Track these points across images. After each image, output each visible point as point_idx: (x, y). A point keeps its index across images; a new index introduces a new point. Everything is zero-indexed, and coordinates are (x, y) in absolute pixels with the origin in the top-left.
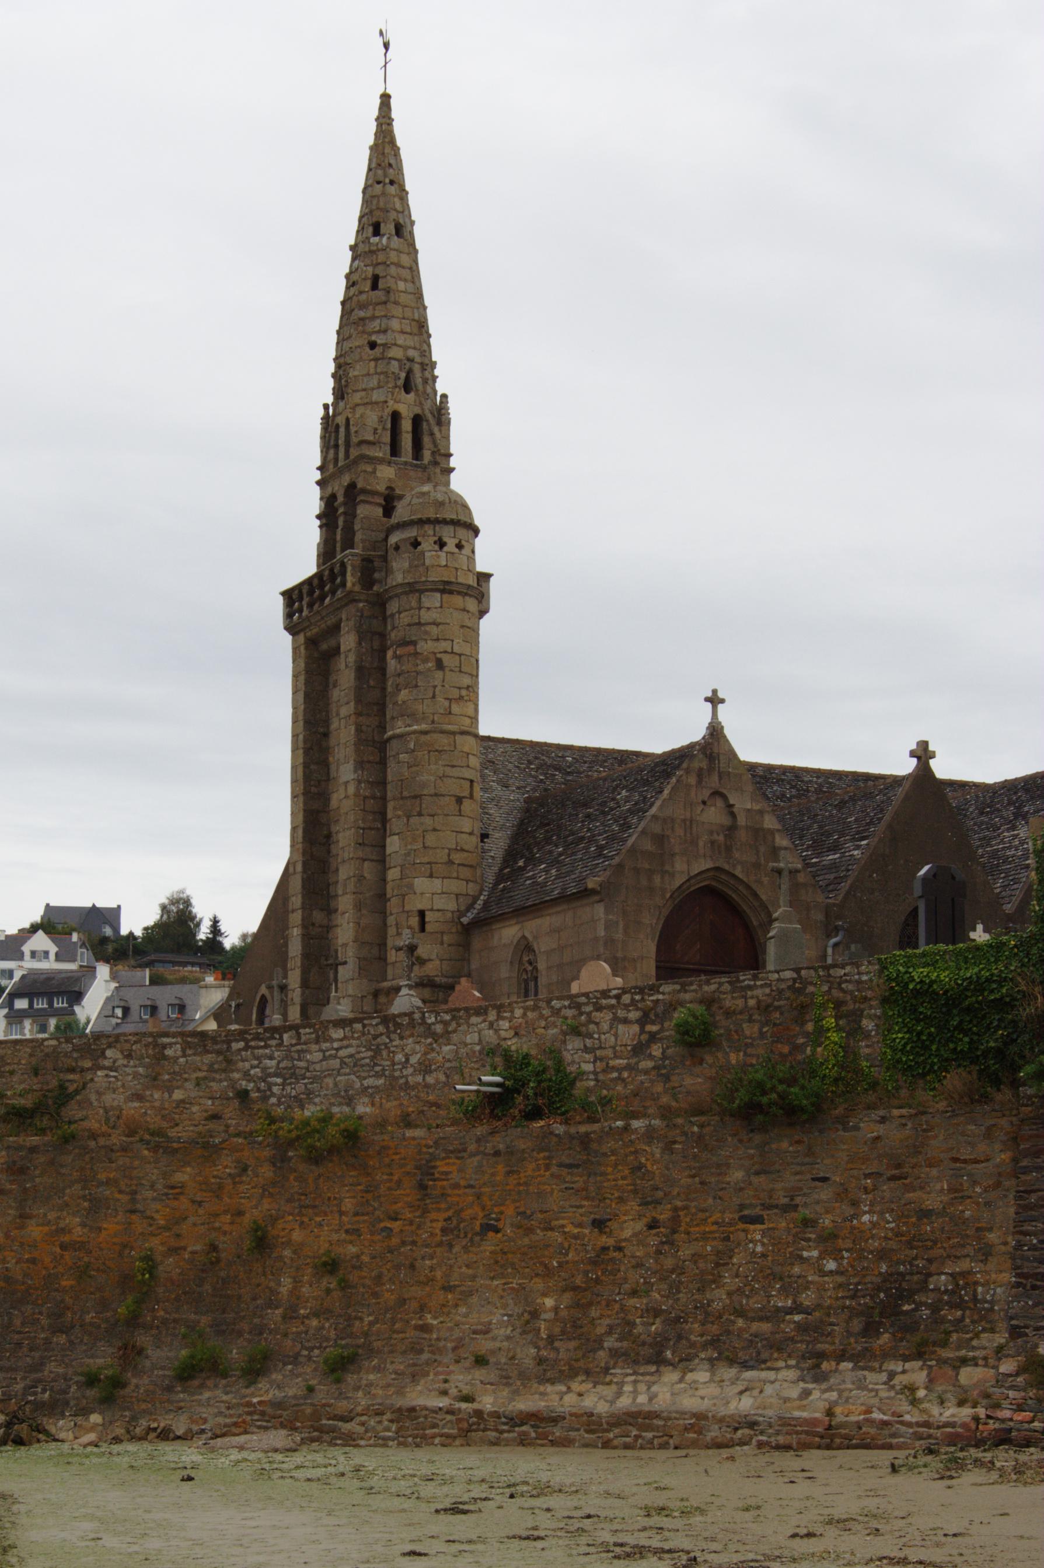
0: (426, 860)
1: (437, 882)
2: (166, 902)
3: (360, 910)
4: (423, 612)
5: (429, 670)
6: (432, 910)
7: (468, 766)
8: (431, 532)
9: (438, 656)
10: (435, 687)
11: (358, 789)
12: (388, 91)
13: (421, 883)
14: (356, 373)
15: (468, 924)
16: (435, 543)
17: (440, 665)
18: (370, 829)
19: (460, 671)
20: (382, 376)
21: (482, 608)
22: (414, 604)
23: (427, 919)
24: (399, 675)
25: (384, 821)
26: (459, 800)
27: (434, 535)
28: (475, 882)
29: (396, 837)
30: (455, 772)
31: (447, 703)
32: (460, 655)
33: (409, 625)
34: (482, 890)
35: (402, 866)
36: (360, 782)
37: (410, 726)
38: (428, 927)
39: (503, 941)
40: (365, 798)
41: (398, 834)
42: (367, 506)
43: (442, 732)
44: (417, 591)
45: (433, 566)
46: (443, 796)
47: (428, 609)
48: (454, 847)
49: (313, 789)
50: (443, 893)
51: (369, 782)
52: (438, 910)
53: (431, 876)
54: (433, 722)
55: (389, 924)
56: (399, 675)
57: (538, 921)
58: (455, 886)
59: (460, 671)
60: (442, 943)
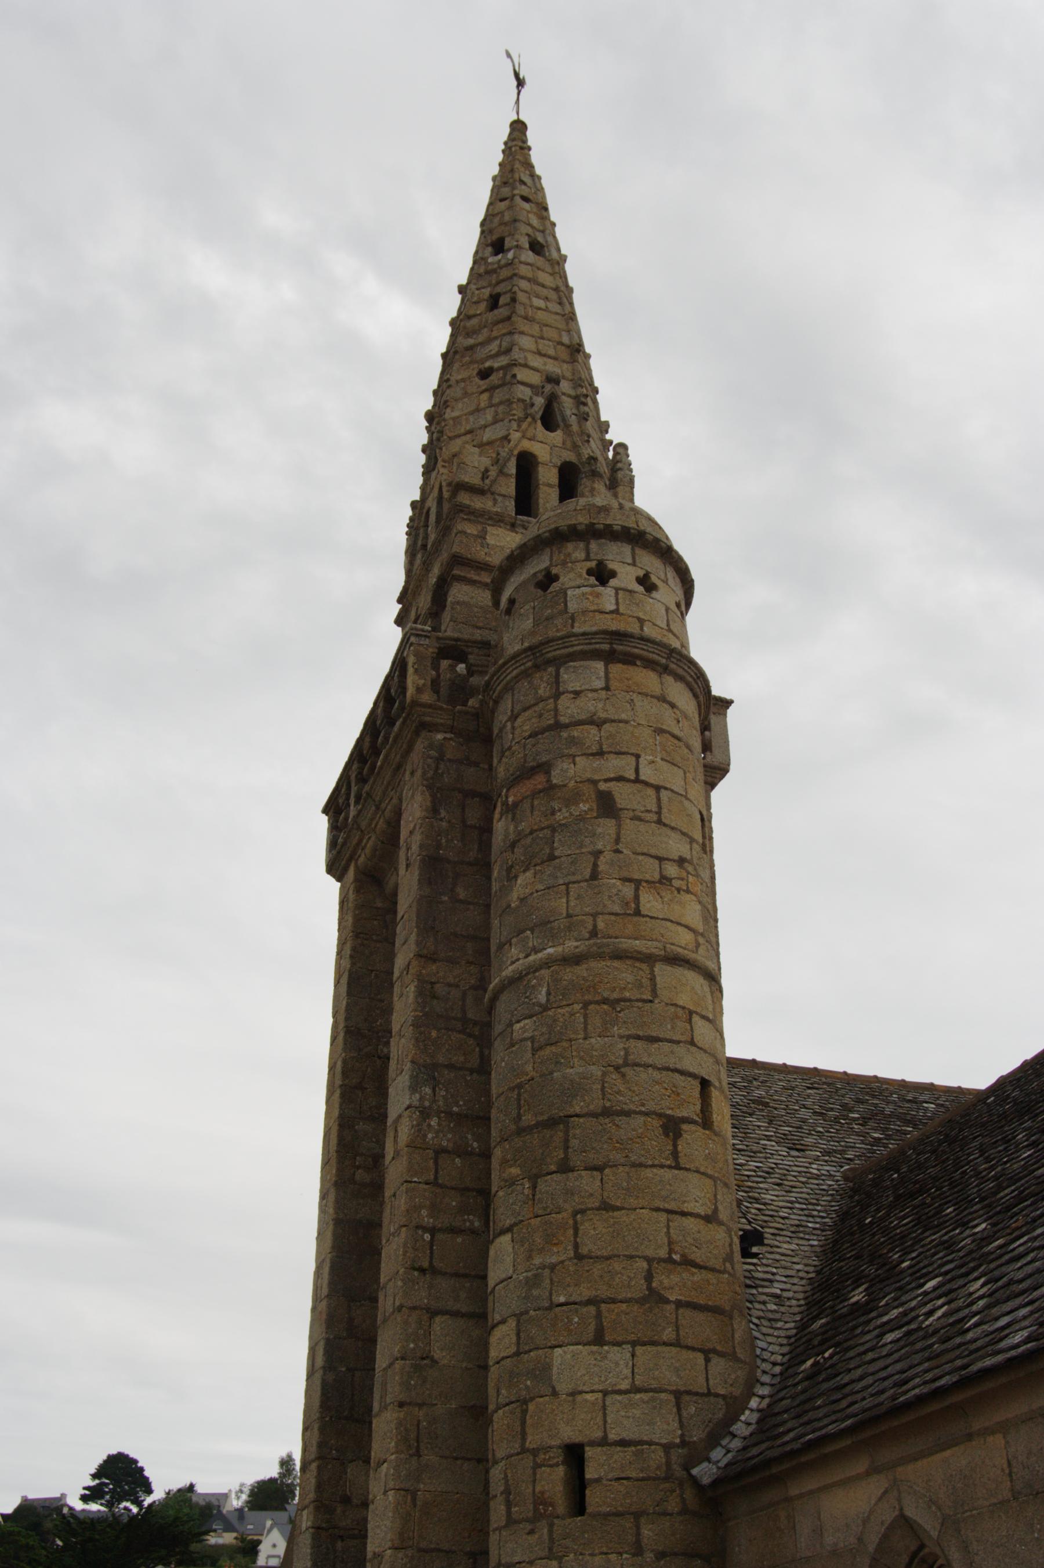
0: (585, 1292)
1: (619, 1356)
2: (139, 1465)
3: (418, 1454)
4: (564, 701)
5: (581, 818)
6: (603, 1442)
7: (692, 1043)
8: (580, 555)
9: (603, 786)
10: (597, 854)
11: (419, 1132)
12: (522, 118)
13: (571, 1363)
14: (456, 414)
15: (716, 1483)
16: (590, 572)
17: (607, 806)
18: (453, 1231)
19: (659, 822)
20: (501, 408)
21: (714, 759)
22: (544, 690)
23: (590, 1474)
24: (513, 845)
25: (482, 1197)
26: (672, 1127)
27: (588, 558)
28: (731, 1356)
29: (506, 1238)
30: (659, 1054)
31: (628, 890)
32: (658, 788)
33: (533, 735)
34: (752, 1382)
35: (518, 1316)
36: (425, 1113)
37: (536, 950)
38: (594, 1499)
39: (829, 1540)
40: (440, 1152)
41: (509, 1230)
42: (466, 588)
43: (619, 956)
44: (549, 662)
45: (584, 612)
46: (628, 1114)
47: (577, 694)
48: (663, 1253)
49: (360, 1175)
50: (636, 1390)
51: (450, 1114)
52: (623, 1443)
53: (599, 1339)
54: (594, 933)
55: (492, 1493)
56: (513, 845)
57: (957, 1458)
58: (670, 1367)
59: (659, 822)
60: (638, 1550)
